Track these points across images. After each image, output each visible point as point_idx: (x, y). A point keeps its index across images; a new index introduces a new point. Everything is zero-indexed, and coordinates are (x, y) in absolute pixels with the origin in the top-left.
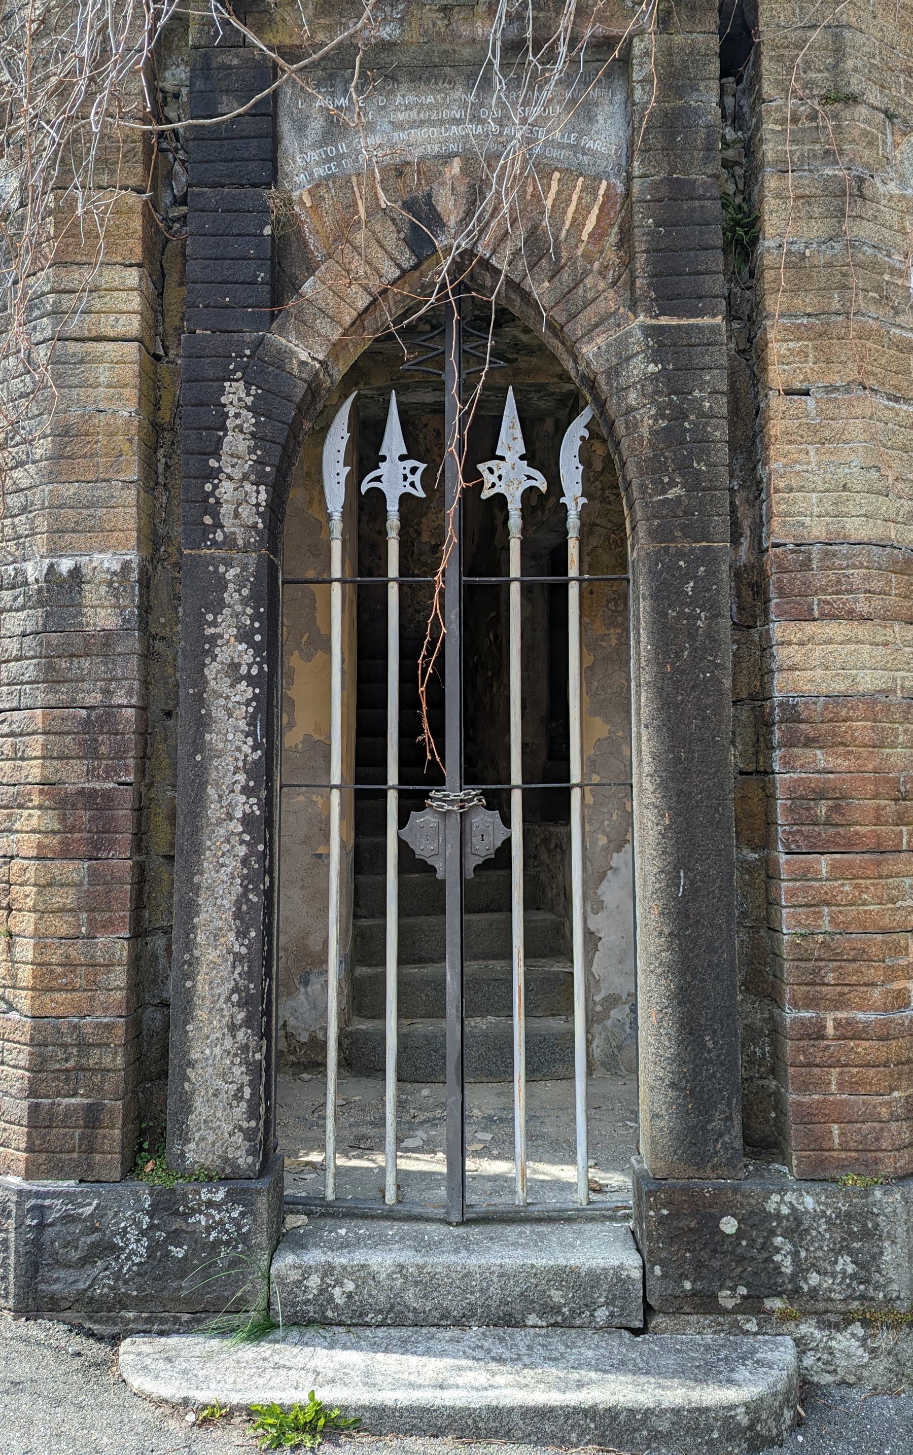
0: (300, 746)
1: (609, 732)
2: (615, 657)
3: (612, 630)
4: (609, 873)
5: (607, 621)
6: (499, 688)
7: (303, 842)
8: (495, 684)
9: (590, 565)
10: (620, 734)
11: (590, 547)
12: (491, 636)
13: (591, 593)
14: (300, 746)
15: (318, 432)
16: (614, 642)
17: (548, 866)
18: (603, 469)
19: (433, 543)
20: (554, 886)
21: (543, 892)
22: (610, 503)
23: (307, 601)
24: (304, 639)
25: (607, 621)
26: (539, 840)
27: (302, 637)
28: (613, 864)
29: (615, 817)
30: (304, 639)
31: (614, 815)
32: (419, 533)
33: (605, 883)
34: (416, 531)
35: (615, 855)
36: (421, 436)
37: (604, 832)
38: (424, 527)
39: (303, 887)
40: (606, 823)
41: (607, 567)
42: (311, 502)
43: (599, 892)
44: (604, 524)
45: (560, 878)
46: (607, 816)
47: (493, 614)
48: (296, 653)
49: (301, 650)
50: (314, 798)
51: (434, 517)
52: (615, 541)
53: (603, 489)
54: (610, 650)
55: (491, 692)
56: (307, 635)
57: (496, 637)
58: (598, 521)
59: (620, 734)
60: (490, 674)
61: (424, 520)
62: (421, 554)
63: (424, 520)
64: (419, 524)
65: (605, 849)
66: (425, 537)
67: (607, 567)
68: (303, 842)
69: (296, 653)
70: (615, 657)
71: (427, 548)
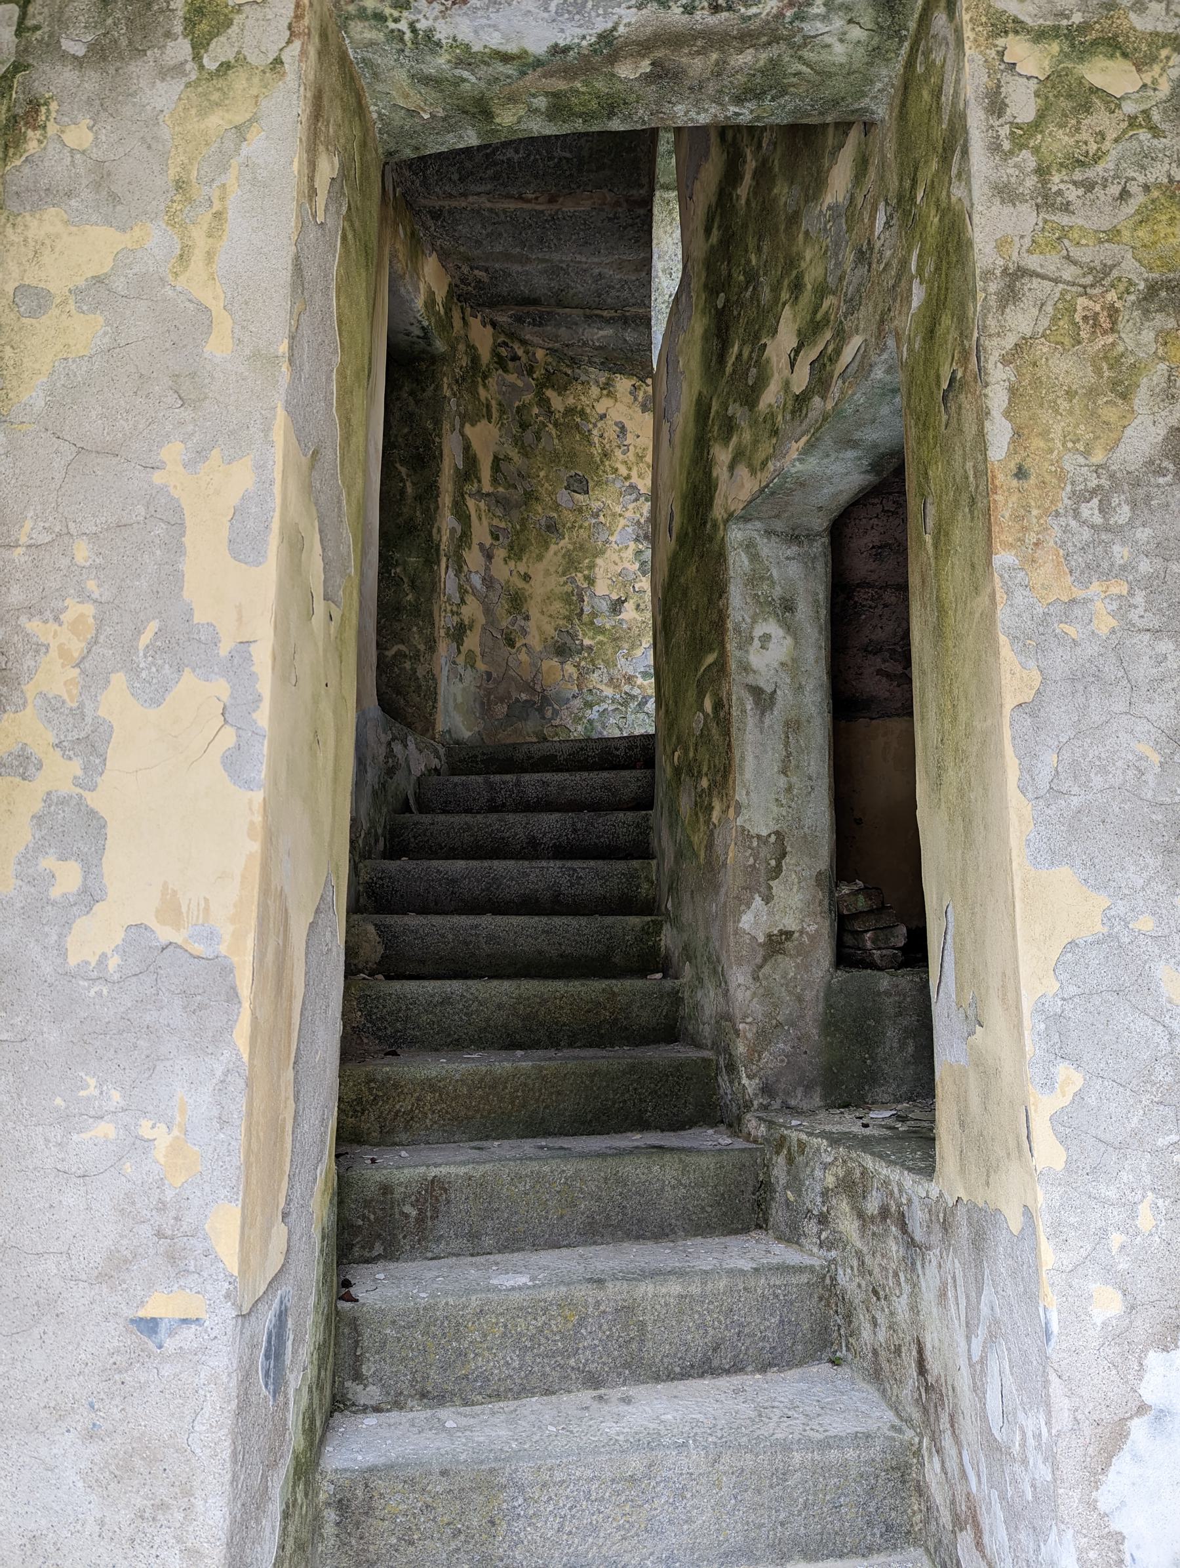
0: (113, 963)
1: (1107, 918)
2: (1111, 671)
3: (1096, 587)
4: (1138, 1428)
5: (1078, 560)
6: (725, 811)
7: (103, 1277)
8: (717, 804)
9: (1013, 391)
10: (1146, 923)
11: (1010, 341)
12: (708, 705)
13: (1021, 473)
14: (113, 963)
15: (212, 76)
16: (1105, 624)
17: (859, 1255)
18: (1041, 115)
19: (615, 597)
20: (881, 1319)
21: (848, 1318)
22: (1066, 208)
23: (160, 529)
24: (145, 639)
25: (1078, 560)
26: (830, 1181)
27: (139, 632)
28: (1148, 1398)
29: (1145, 1219)
30: (145, 639)
31: (1144, 1210)
32: (591, 581)
33: (1122, 1463)
34: (587, 578)
35: (1154, 1358)
36: (595, 432)
37: (1109, 1273)
38: (599, 572)
39: (92, 1434)
40: (1117, 1239)
41: (1070, 394)
42: (184, 257)
43: (1105, 1499)
44: (1051, 269)
45: (901, 1304)
46: (1117, 1215)
47: (710, 659)
48: (119, 680)
49: (134, 671)
50: (145, 1129)
51: (615, 557)
52: (1093, 319)
53: (1042, 172)
54: (1092, 649)
55: (708, 821)
56: (154, 626)
57: (718, 705)
58: (1032, 262)
59: (1146, 923)
60: (705, 783)
61: (599, 561)
62: (594, 615)
63: (599, 561)
64: (592, 567)
65: (1117, 1335)
66: (601, 588)
67: (1070, 394)
68: (103, 1277)
69: (119, 680)
70: (1111, 671)
71: (604, 606)
